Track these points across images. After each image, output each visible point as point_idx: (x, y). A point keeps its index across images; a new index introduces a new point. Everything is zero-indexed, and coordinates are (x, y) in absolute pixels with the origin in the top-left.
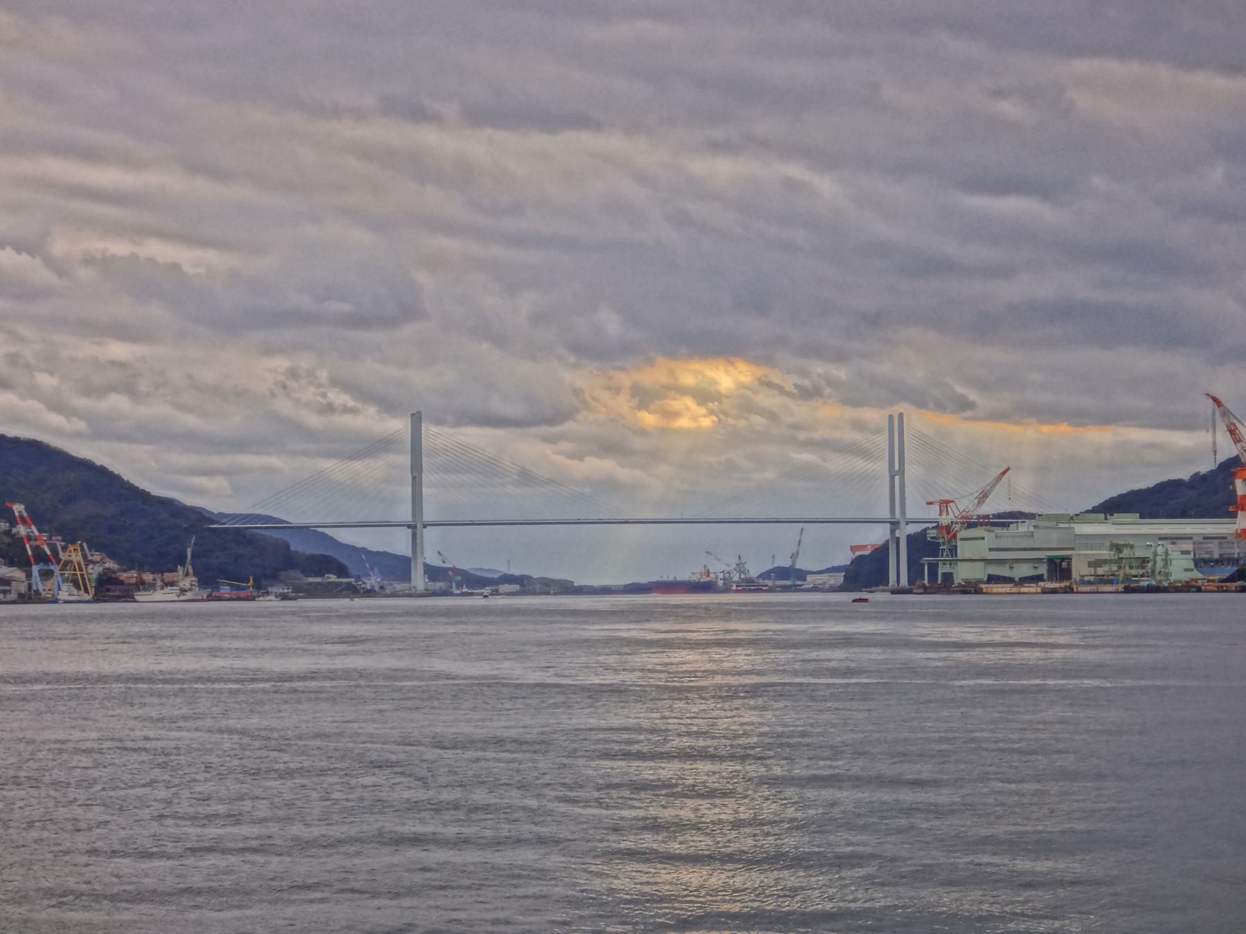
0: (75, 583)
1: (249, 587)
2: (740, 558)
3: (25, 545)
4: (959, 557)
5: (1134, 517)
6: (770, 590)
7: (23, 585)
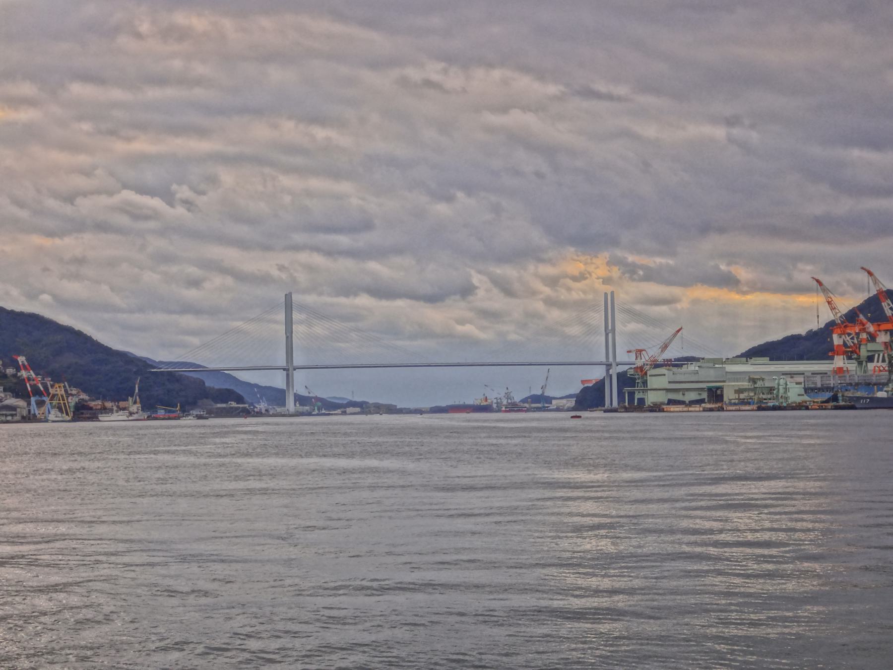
4: (649, 387)
5: (766, 360)
6: (528, 410)
7: (25, 411)
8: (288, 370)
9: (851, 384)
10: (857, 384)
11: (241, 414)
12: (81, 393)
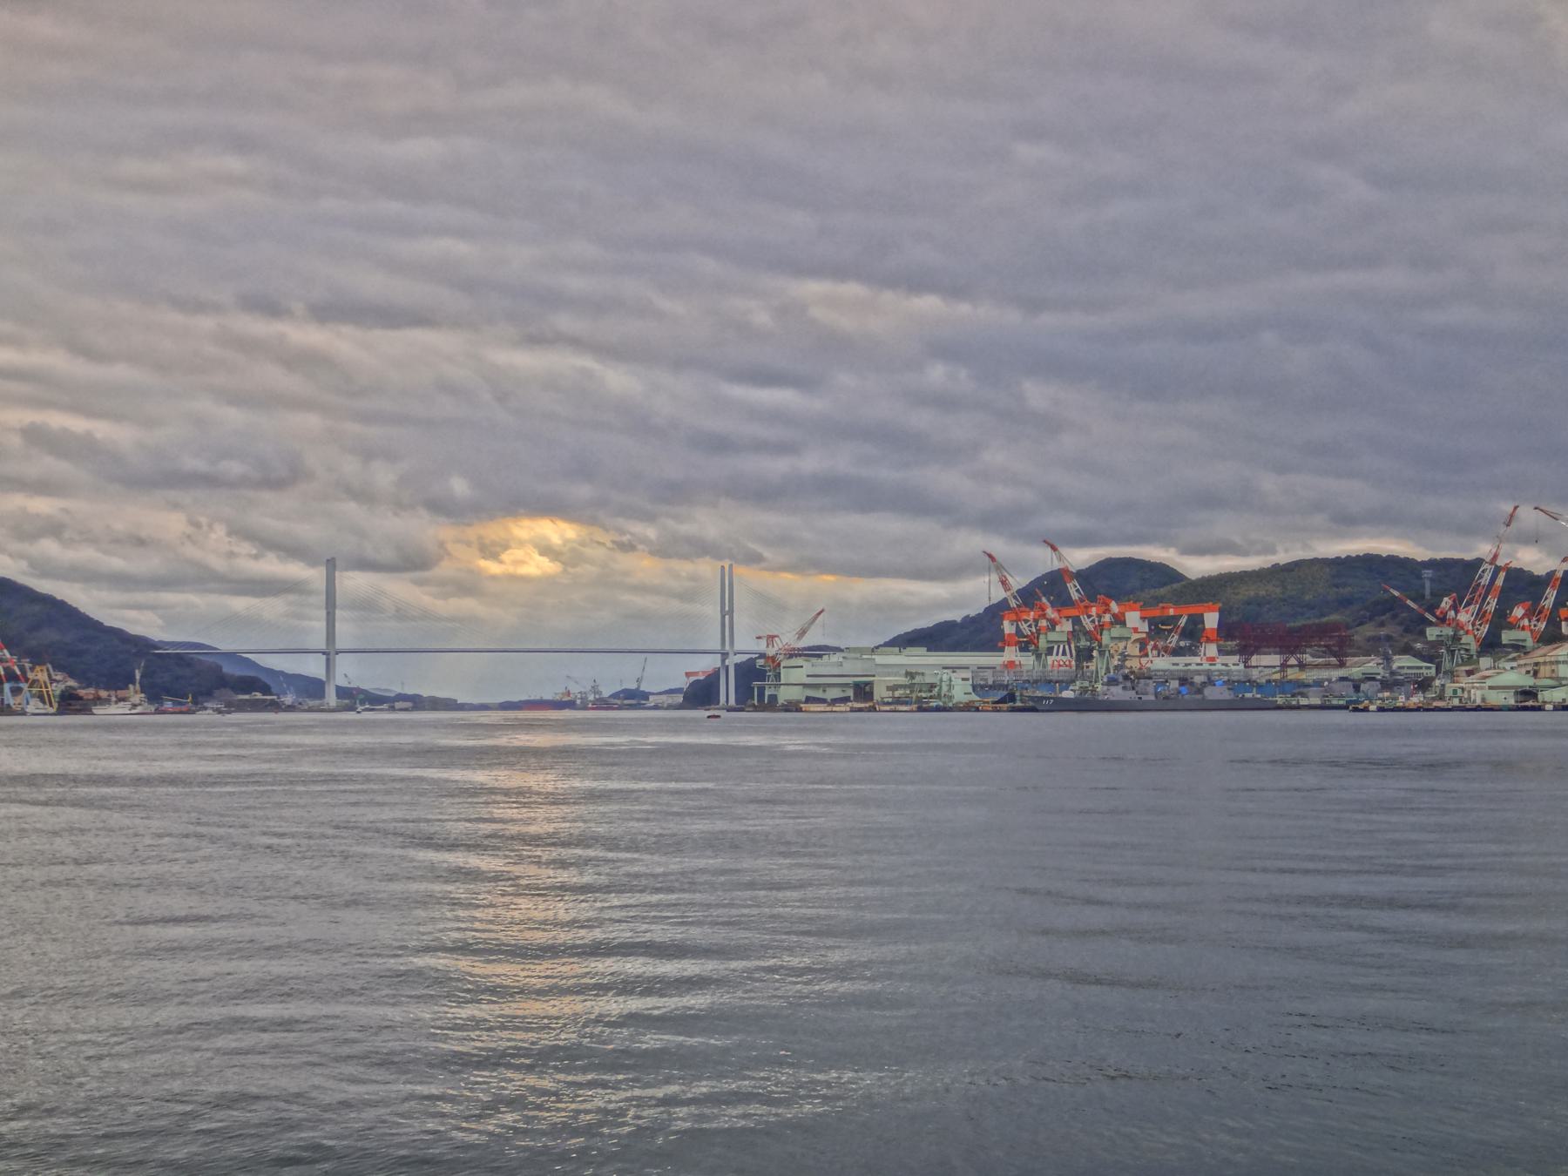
4: (782, 682)
5: (923, 650)
6: (620, 708)
8: (329, 654)
9: (1028, 681)
10: (1036, 682)
11: (269, 708)
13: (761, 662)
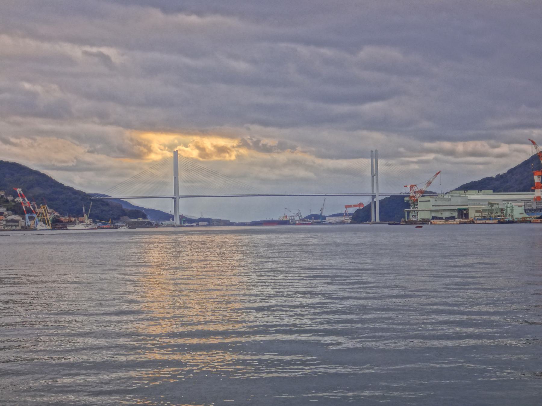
0: (45, 223)
1: (109, 223)
2: (299, 210)
3: (22, 206)
4: (419, 208)
6: (312, 224)
7: (23, 223)
11: (147, 225)
12: (54, 212)
13: (406, 199)
